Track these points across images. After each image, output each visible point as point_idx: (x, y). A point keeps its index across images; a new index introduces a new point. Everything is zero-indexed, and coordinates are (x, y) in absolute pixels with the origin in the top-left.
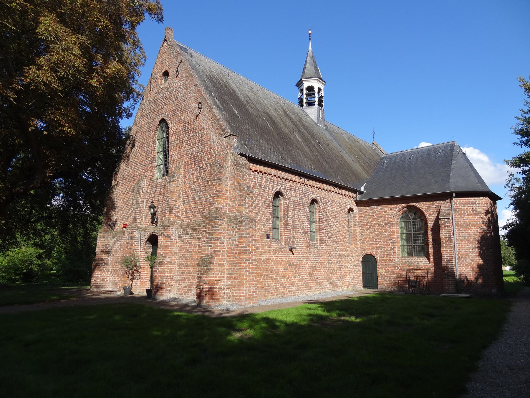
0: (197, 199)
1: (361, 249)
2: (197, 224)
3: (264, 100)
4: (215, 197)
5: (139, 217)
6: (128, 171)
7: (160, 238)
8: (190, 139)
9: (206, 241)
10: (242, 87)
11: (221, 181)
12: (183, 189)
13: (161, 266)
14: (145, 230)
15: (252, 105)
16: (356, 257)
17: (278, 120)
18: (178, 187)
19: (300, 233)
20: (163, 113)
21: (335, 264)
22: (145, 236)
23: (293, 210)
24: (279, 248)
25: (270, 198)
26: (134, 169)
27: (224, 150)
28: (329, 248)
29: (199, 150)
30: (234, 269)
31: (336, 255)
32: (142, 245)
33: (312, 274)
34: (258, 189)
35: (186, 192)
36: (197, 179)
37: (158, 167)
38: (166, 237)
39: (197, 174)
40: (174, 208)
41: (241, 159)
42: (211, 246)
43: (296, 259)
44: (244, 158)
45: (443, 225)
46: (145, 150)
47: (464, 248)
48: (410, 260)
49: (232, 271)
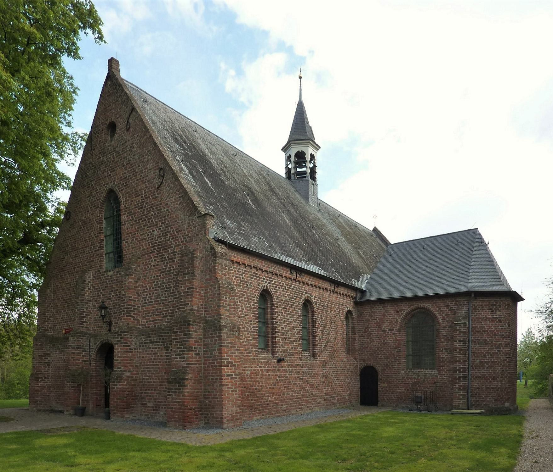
0: (162, 298)
1: (360, 359)
2: (163, 330)
3: (243, 169)
4: (187, 295)
5: (86, 320)
6: (67, 260)
7: (116, 347)
8: (150, 219)
9: (177, 352)
10: (214, 149)
11: (194, 276)
12: (142, 285)
13: (120, 382)
14: (95, 336)
15: (228, 175)
16: (353, 369)
17: (261, 197)
18: (137, 282)
19: (291, 341)
20: (111, 182)
21: (330, 378)
22: (95, 344)
23: (282, 313)
24: (265, 359)
25: (255, 297)
26: (74, 258)
27: (197, 235)
28: (323, 358)
29: (163, 233)
30: (213, 385)
31: (331, 367)
32: (92, 355)
33: (304, 390)
34: (241, 286)
35: (147, 289)
36: (161, 273)
37: (107, 255)
38: (124, 346)
39: (161, 266)
40: (132, 309)
41: (220, 247)
42: (184, 358)
43: (285, 372)
44: (223, 247)
45: (458, 331)
46: (88, 233)
47: (479, 357)
48: (416, 372)
49: (211, 389)
